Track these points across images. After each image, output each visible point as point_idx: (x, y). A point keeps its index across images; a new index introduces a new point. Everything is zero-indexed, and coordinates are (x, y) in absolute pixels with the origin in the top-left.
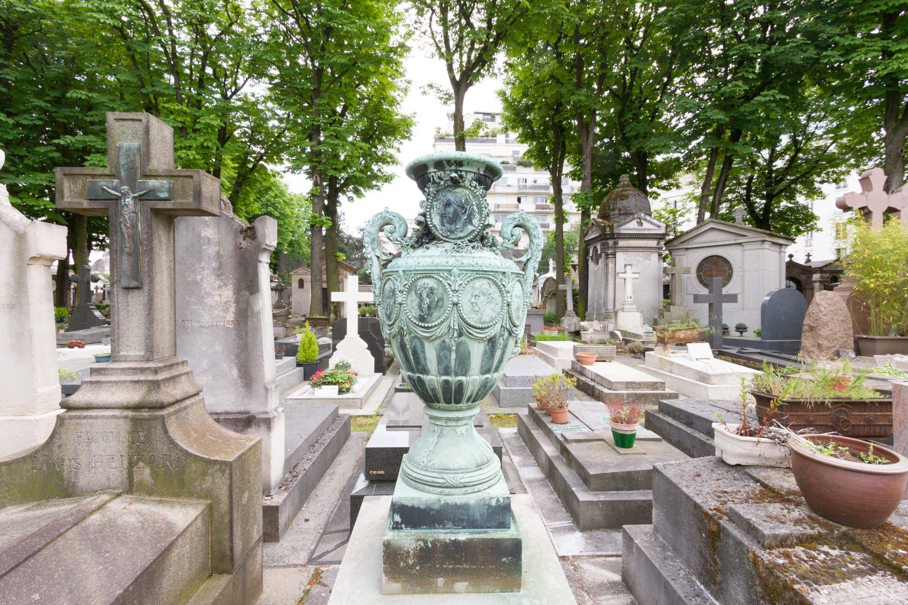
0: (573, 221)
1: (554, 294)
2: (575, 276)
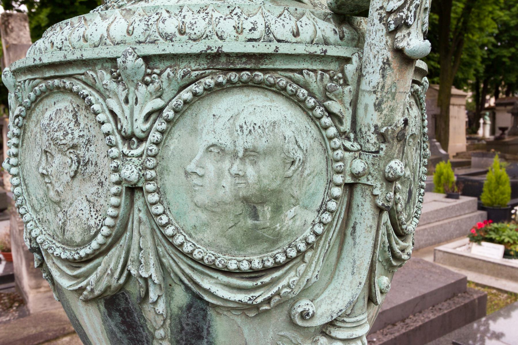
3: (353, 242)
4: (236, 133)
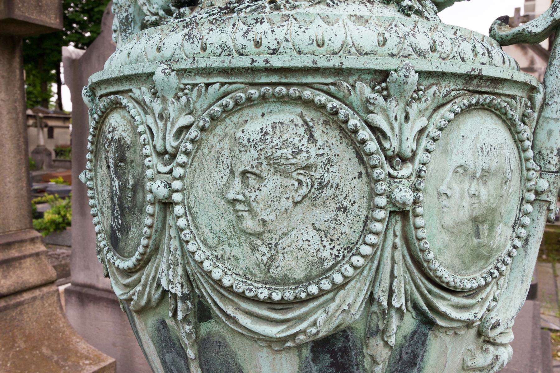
3: (524, 253)
4: (477, 154)
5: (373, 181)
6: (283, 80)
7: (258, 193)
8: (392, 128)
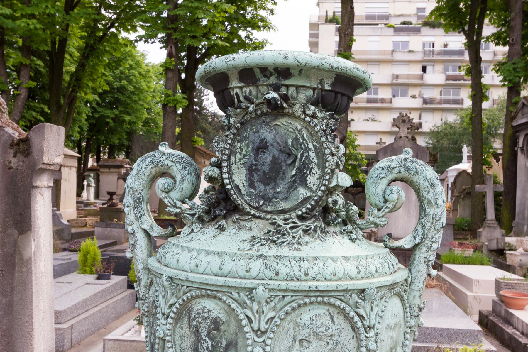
0: (497, 94)
1: (469, 194)
2: (497, 169)
5: (359, 340)
6: (321, 295)
7: (308, 350)
8: (367, 315)
